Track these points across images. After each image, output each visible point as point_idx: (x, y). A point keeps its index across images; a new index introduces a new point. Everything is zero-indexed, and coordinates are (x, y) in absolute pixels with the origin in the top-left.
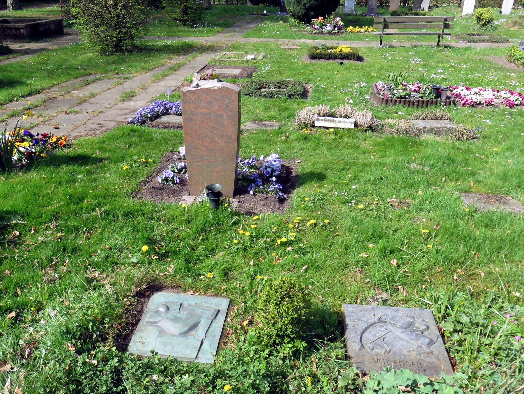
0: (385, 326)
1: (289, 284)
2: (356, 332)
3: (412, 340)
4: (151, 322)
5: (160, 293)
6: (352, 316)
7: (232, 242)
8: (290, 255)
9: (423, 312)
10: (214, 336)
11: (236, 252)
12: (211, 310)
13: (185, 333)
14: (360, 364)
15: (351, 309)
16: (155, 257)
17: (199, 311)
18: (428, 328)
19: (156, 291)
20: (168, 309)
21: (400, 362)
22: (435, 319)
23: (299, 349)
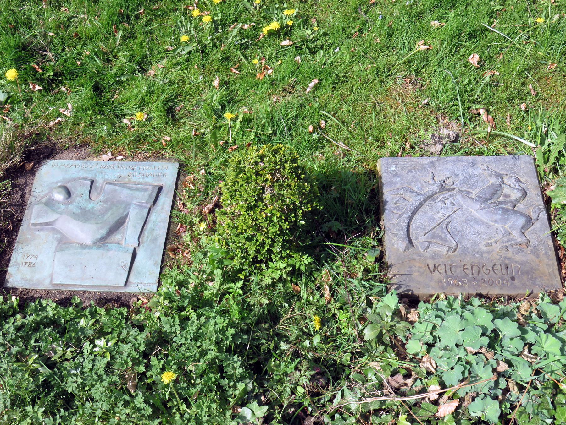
0: (450, 199)
1: (272, 165)
2: (400, 216)
3: (495, 221)
4: (41, 224)
5: (52, 162)
6: (395, 183)
7: (178, 38)
8: (287, 58)
9: (518, 163)
10: (155, 240)
11: (188, 60)
12: (146, 190)
13: (102, 241)
14: (403, 278)
15: (393, 168)
16: (37, 87)
17: (124, 194)
18: (525, 194)
19: (44, 158)
20: (69, 194)
21: (472, 266)
22: (538, 173)
23: (299, 269)
